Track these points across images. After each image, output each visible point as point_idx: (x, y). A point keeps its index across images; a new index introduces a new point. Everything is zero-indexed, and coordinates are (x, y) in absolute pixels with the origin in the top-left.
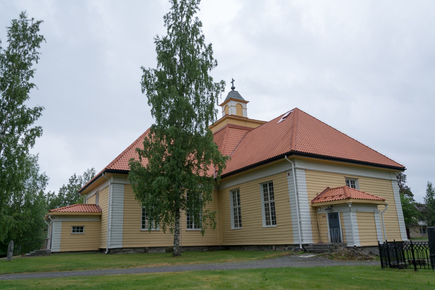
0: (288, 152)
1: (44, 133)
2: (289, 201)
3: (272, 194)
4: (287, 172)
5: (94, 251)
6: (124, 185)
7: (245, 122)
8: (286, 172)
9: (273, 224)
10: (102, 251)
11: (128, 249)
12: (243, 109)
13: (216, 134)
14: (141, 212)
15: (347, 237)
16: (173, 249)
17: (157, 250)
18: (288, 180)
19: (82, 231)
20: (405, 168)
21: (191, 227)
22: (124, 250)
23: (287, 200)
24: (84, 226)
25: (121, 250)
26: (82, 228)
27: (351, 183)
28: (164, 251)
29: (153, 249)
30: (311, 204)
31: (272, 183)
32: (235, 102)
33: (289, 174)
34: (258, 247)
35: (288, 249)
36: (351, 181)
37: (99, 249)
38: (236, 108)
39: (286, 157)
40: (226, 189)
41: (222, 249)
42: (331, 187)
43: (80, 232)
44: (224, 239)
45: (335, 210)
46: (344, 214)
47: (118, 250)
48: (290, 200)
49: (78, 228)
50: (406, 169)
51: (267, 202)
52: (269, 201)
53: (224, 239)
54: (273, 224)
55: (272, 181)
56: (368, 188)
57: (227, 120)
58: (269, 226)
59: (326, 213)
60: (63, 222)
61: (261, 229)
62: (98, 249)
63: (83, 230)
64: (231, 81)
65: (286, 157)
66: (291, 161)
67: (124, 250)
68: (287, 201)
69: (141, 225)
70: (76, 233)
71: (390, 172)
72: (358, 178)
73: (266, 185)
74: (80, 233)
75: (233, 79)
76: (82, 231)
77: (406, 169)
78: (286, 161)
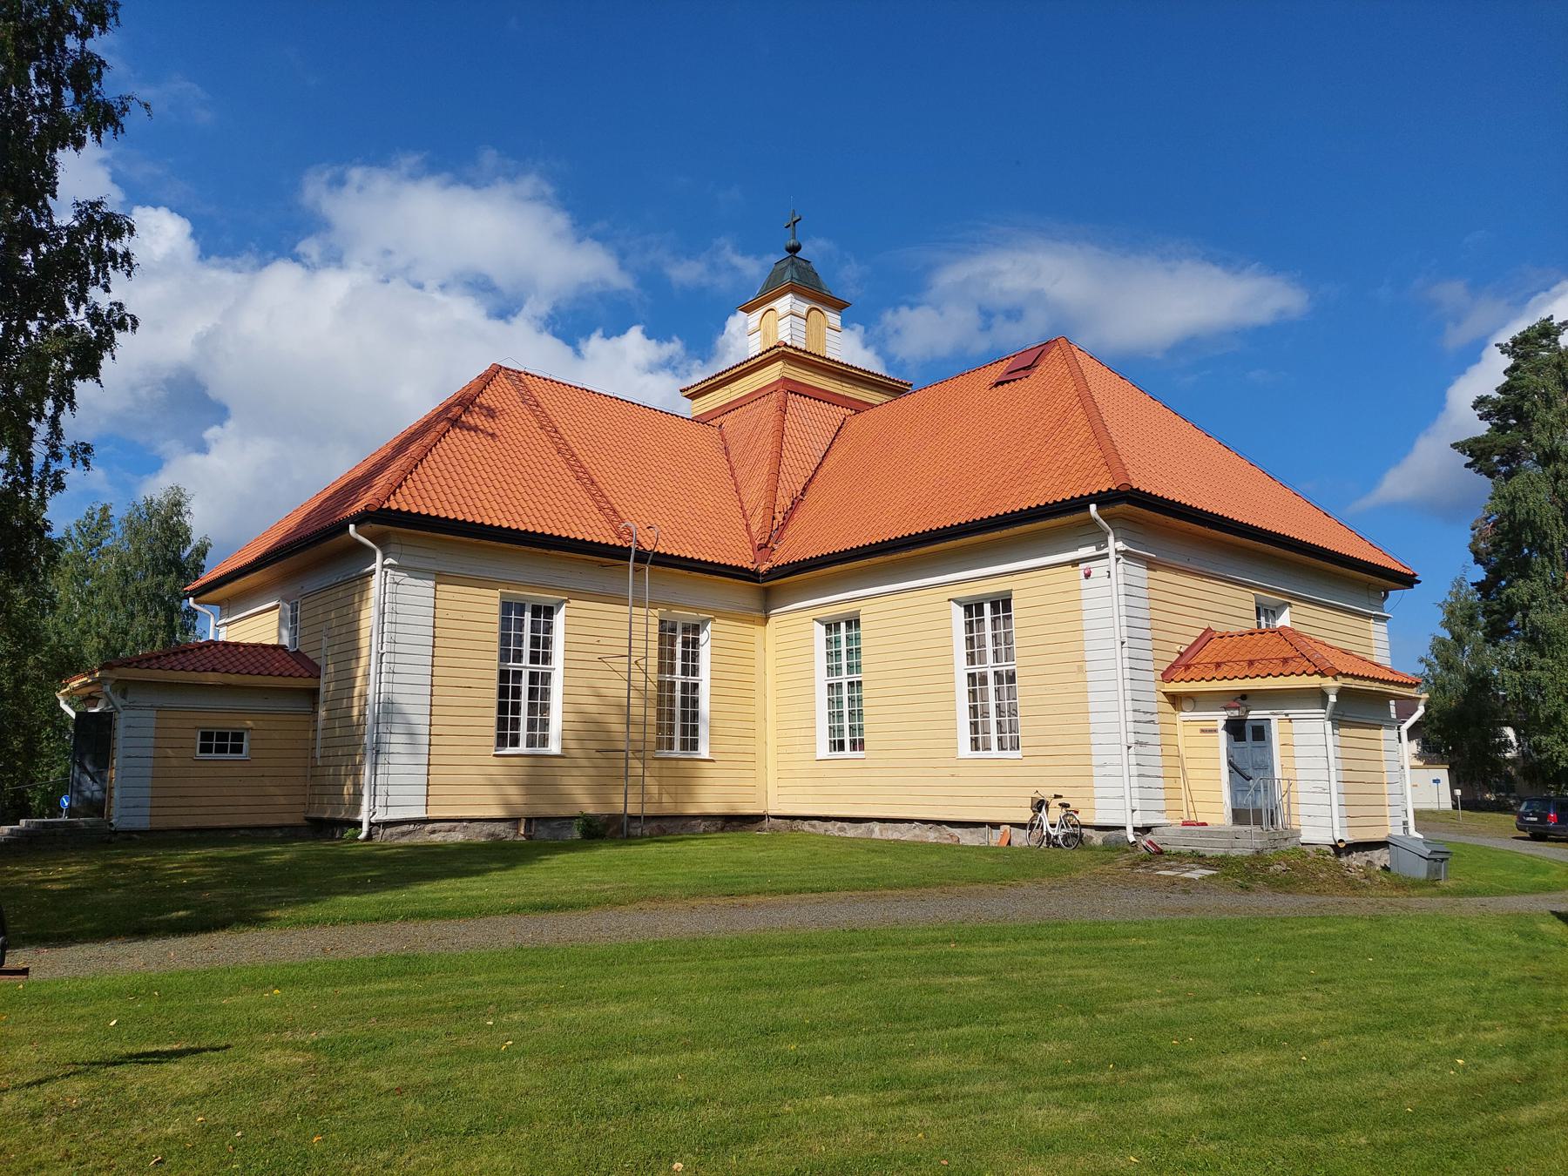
1: (230, 425)
2: (1081, 670)
3: (854, 653)
4: (1082, 566)
8: (1075, 563)
9: (854, 748)
14: (495, 684)
15: (1302, 810)
16: (87, 799)
18: (1084, 594)
19: (237, 749)
20: (1417, 578)
23: (1074, 667)
25: (422, 826)
26: (238, 737)
31: (857, 622)
33: (1087, 576)
37: (307, 819)
42: (1219, 628)
48: (1088, 666)
49: (222, 736)
50: (1419, 582)
51: (835, 680)
52: (844, 678)
54: (854, 748)
58: (981, 754)
60: (159, 709)
63: (245, 744)
68: (1076, 669)
69: (493, 731)
70: (214, 755)
71: (1368, 589)
73: (838, 625)
74: (228, 755)
76: (237, 749)
77: (1419, 582)
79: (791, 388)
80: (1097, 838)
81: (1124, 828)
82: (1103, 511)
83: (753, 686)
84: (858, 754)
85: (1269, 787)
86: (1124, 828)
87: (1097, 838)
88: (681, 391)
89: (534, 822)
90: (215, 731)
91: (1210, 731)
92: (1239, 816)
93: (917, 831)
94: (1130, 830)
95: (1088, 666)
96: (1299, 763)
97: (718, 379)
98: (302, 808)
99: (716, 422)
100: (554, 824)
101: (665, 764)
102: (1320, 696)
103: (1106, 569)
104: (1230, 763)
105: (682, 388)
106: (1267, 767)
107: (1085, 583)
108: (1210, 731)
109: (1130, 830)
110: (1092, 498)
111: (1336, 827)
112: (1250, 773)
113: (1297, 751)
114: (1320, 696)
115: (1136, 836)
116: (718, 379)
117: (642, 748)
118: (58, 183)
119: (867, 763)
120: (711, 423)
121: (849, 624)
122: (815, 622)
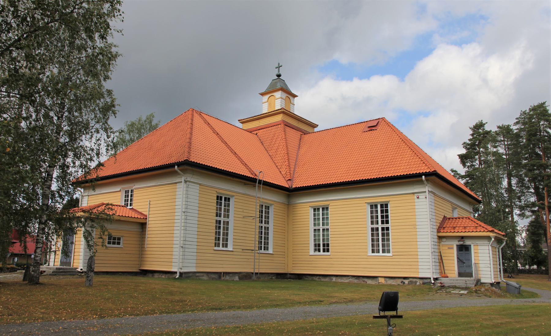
0: (181, 161)
4: (416, 195)
5: (265, 275)
6: (199, 186)
7: (258, 121)
8: (413, 193)
10: (145, 273)
11: (202, 274)
12: (291, 104)
13: (261, 131)
15: (481, 272)
17: (230, 277)
18: (416, 204)
19: (119, 243)
21: (319, 251)
22: (197, 274)
23: (412, 227)
24: (122, 236)
27: (265, 209)
28: (237, 278)
29: (226, 275)
30: (436, 234)
31: (327, 208)
32: (284, 93)
33: (418, 198)
34: (356, 279)
35: (408, 282)
36: (266, 206)
37: (140, 270)
38: (284, 101)
39: (176, 167)
40: (298, 205)
41: (296, 279)
43: (111, 245)
44: (294, 265)
45: (468, 242)
46: (479, 247)
47: (190, 275)
53: (294, 265)
55: (389, 202)
56: (338, 218)
57: (282, 114)
59: (455, 244)
61: (365, 257)
62: (139, 271)
63: (121, 241)
64: (277, 66)
65: (176, 167)
66: (182, 172)
67: (197, 274)
72: (457, 208)
73: (319, 209)
74: (116, 246)
75: (279, 64)
76: (119, 243)
78: (422, 181)
79: (287, 125)
80: (419, 282)
81: (430, 278)
82: (426, 178)
83: (432, 226)
84: (326, 253)
85: (470, 266)
86: (430, 278)
87: (419, 282)
88: (239, 120)
89: (225, 274)
90: (117, 237)
91: (451, 248)
92: (460, 275)
93: (351, 280)
94: (432, 279)
95: (417, 227)
96: (480, 258)
97: (255, 118)
98: (138, 266)
99: (255, 132)
100: (231, 275)
101: (261, 255)
102: (489, 238)
103: (425, 196)
104: (458, 258)
105: (239, 119)
106: (470, 260)
107: (417, 200)
108: (451, 248)
109: (432, 279)
110: (423, 174)
111: (493, 278)
112: (464, 261)
113: (480, 255)
114: (489, 238)
115: (434, 281)
116: (255, 118)
117: (254, 249)
118: (499, 127)
119: (331, 257)
120: (253, 132)
121: (323, 209)
122: (310, 207)
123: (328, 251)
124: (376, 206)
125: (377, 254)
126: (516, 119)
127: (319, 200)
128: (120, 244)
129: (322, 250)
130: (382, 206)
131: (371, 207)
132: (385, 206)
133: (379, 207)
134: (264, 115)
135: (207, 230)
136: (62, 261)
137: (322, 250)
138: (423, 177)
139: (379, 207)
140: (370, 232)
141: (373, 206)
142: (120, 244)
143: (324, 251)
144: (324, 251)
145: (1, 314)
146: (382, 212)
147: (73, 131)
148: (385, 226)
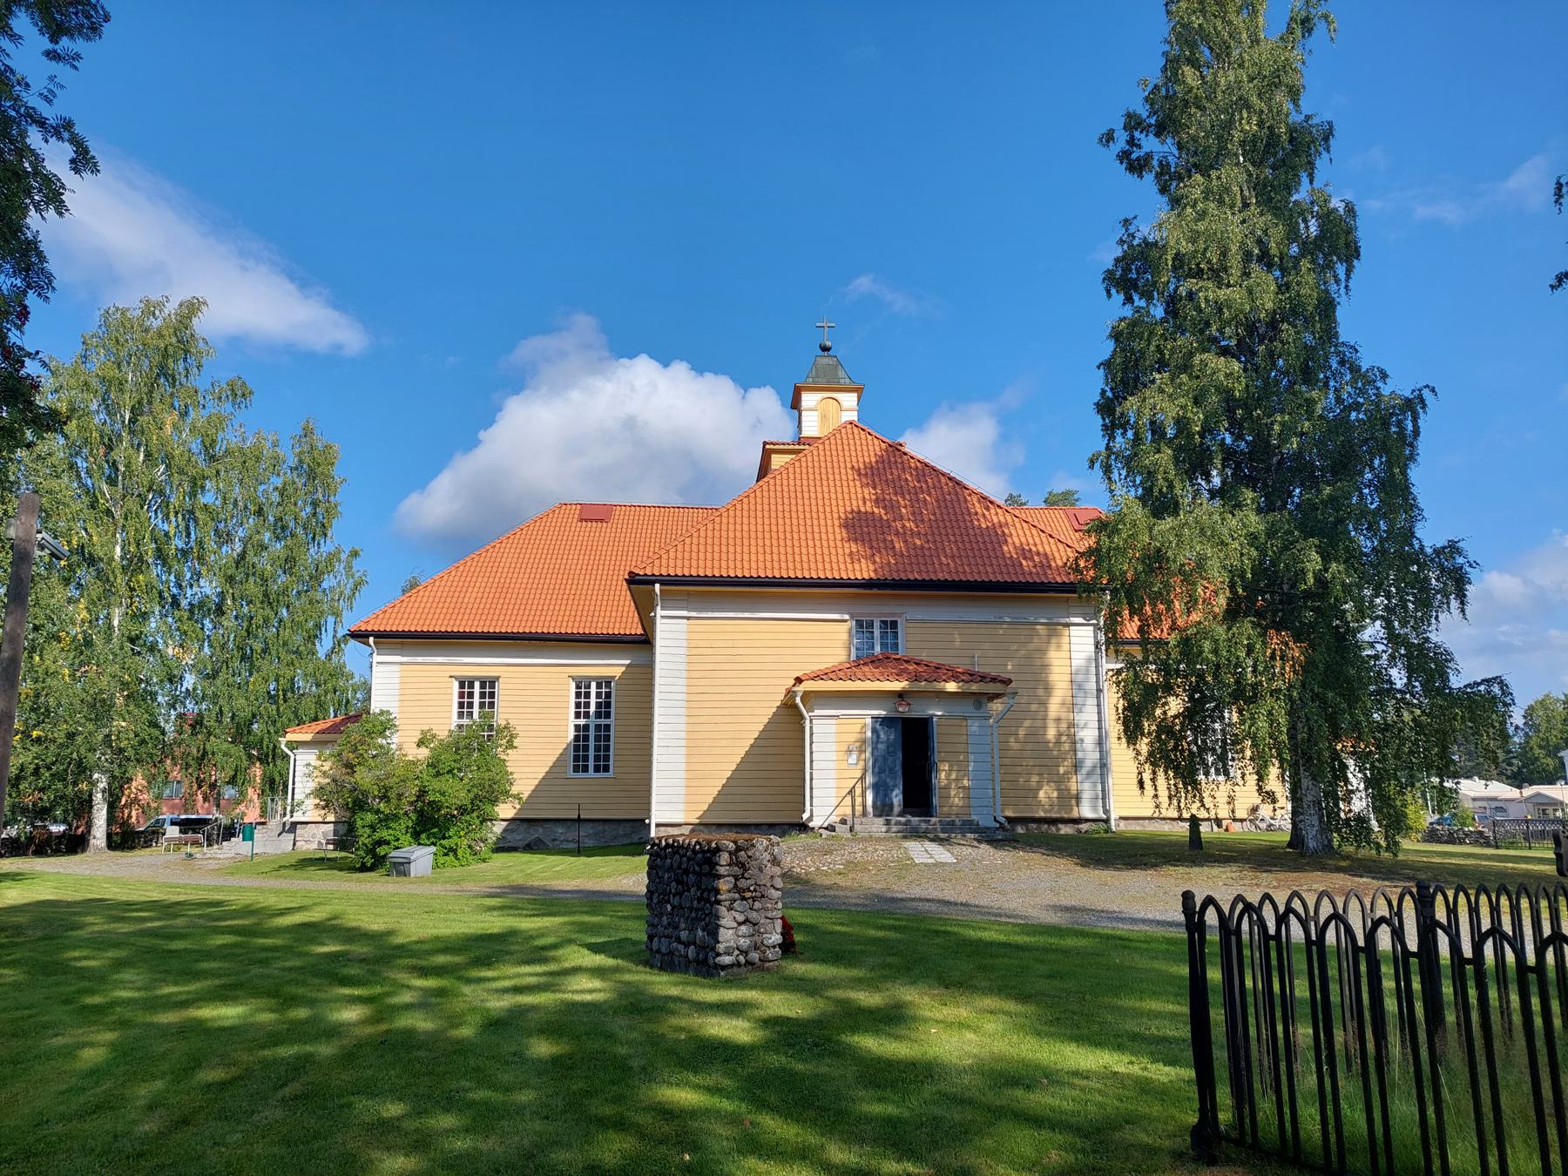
21: (585, 769)
55: (498, 678)
84: (602, 774)
123: (606, 769)
124: (471, 685)
125: (585, 775)
126: (1092, 466)
127: (478, 665)
128: (608, 771)
129: (591, 768)
130: (483, 685)
131: (462, 685)
132: (489, 684)
133: (477, 684)
134: (782, 447)
135: (728, 682)
136: (637, 932)
137: (591, 768)
138: (657, 586)
139: (477, 684)
140: (613, 710)
141: (465, 684)
142: (608, 771)
143: (597, 769)
144: (597, 769)
145: (1462, 1153)
146: (482, 695)
147: (1358, 420)
148: (603, 721)
